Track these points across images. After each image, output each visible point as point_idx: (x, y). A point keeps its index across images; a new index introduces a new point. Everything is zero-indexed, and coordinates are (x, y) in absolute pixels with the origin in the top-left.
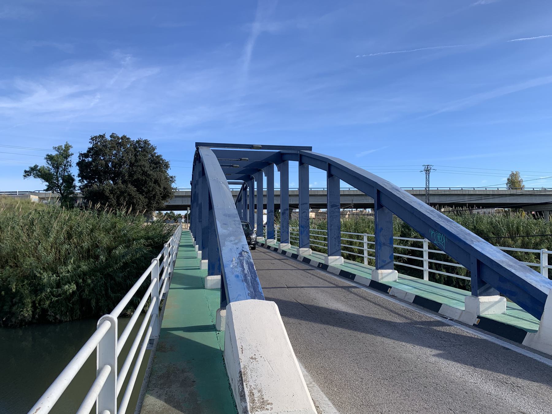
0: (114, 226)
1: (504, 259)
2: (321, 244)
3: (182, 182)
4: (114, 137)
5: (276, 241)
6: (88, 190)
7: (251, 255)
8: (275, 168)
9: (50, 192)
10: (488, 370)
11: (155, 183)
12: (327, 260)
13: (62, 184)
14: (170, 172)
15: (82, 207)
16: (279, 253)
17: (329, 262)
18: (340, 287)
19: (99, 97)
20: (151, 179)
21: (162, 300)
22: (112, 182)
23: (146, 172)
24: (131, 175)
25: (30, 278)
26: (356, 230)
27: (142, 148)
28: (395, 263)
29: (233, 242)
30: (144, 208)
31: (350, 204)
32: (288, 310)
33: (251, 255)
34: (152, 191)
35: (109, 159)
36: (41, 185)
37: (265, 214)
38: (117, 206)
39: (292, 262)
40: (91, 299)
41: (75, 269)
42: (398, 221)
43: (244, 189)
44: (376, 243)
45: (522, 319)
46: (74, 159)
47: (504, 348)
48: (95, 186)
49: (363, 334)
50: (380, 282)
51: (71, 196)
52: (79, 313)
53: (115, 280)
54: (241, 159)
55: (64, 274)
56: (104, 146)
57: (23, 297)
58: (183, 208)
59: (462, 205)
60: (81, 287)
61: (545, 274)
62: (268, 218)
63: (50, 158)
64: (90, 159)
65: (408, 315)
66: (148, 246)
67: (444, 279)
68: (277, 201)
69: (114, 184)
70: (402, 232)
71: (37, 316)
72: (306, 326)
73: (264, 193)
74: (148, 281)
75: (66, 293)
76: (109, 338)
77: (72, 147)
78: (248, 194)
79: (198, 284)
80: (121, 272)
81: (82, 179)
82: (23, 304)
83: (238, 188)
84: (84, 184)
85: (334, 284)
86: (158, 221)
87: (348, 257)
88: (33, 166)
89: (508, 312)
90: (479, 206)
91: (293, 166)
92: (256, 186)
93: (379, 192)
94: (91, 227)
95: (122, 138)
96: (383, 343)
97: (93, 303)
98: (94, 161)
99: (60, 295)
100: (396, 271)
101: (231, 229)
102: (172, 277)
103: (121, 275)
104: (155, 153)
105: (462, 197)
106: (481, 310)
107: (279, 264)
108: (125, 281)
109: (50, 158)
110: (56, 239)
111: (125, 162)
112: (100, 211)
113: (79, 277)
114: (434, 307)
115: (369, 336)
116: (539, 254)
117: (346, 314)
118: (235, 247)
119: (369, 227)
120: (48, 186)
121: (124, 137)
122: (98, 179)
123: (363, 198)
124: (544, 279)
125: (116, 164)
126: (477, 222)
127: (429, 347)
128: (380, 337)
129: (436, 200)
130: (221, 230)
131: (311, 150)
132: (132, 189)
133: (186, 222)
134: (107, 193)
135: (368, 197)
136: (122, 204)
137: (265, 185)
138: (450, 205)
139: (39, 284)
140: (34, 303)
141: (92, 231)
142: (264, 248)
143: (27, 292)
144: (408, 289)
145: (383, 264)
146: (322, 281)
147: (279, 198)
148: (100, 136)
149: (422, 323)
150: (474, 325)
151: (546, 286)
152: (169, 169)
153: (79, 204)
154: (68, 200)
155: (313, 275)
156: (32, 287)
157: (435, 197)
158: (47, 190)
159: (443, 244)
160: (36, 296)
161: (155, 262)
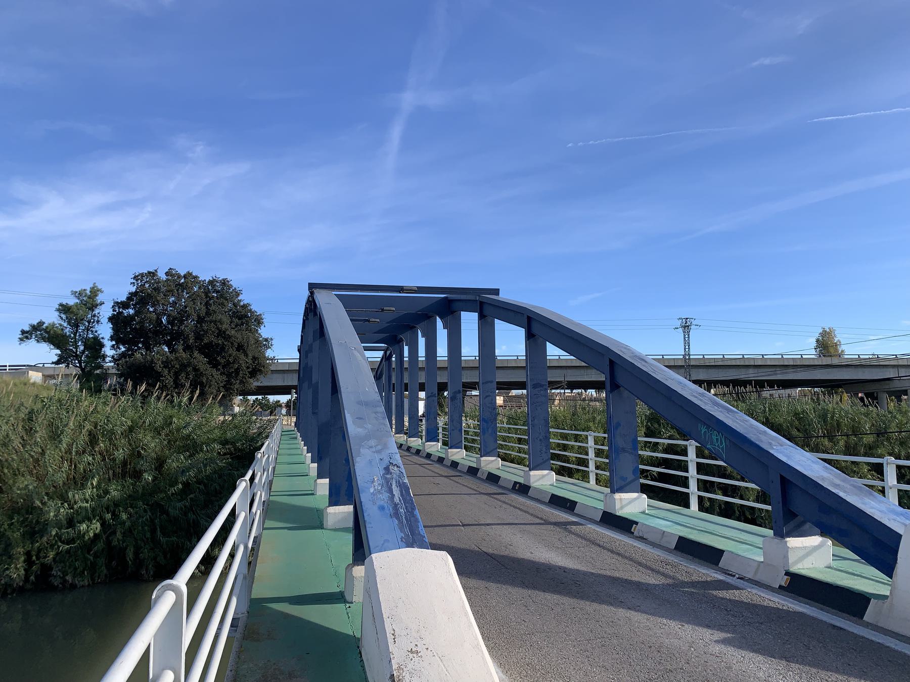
0: (168, 422)
1: (825, 474)
2: (513, 449)
3: (283, 346)
4: (172, 275)
5: (440, 444)
6: (126, 362)
7: (404, 471)
8: (439, 323)
9: (63, 366)
10: (809, 665)
11: (238, 349)
12: (528, 477)
13: (83, 352)
14: (264, 332)
15: (115, 390)
16: (447, 466)
17: (532, 481)
18: (551, 523)
19: (150, 209)
20: (232, 344)
21: (253, 549)
22: (166, 349)
23: (224, 332)
24: (198, 337)
25: (23, 511)
26: (574, 427)
27: (218, 292)
28: (642, 481)
29: (374, 449)
30: (219, 391)
32: (475, 566)
33: (404, 471)
34: (234, 362)
35: (161, 312)
36: (47, 354)
37: (422, 400)
38: (175, 388)
39: (469, 480)
40: (127, 546)
41: (99, 496)
42: (642, 409)
43: (387, 358)
44: (610, 448)
45: (861, 577)
46: (105, 312)
47: (834, 626)
48: (138, 355)
49: (595, 606)
50: (618, 514)
51: (98, 372)
52: (105, 571)
53: (168, 514)
54: (383, 310)
55: (80, 504)
56: (155, 289)
57: (11, 544)
58: (285, 390)
59: (744, 383)
60: (109, 525)
61: (893, 497)
62: (427, 406)
63: (64, 309)
64: (131, 311)
65: (669, 571)
66: (225, 454)
67: (720, 506)
68: (442, 378)
69: (171, 352)
70: (648, 428)
71: (32, 578)
72: (504, 595)
74: (233, 515)
75: (84, 537)
76: (173, 622)
77: (102, 292)
78: (394, 366)
79: (312, 520)
80: (180, 501)
81: (117, 343)
82: (10, 557)
83: (377, 356)
84: (119, 352)
85: (541, 519)
86: (242, 414)
87: (560, 471)
88: (35, 323)
89: (835, 564)
90: (772, 384)
91: (469, 321)
92: (406, 353)
93: (612, 363)
94: (129, 423)
95: (185, 277)
96: (630, 619)
97: (130, 554)
98: (137, 313)
99: (72, 541)
100: (645, 496)
101: (370, 426)
102: (270, 509)
103: (179, 505)
104: (240, 301)
105: (743, 370)
107: (446, 485)
108: (185, 514)
109: (64, 309)
110: (70, 446)
111: (188, 316)
112: (145, 398)
113: (104, 509)
114: (711, 556)
115: (605, 609)
117: (565, 570)
118: (377, 457)
120: (59, 356)
121: (188, 275)
122: (143, 343)
123: (582, 371)
124: (892, 507)
125: (175, 319)
126: (770, 410)
127: (708, 627)
128: (624, 611)
129: (702, 375)
130: (353, 428)
131: (498, 294)
132: (200, 360)
133: (288, 414)
134: (158, 367)
135: (589, 371)
136: (183, 386)
137: (422, 352)
138: (725, 383)
139: (38, 522)
140: (28, 554)
141: (131, 429)
142: (421, 457)
143: (17, 535)
144: (666, 527)
146: (519, 512)
147: (446, 373)
148: (149, 273)
149: (693, 584)
150: (781, 587)
151: (898, 519)
152: (262, 327)
153: (110, 385)
154: (91, 379)
155: (504, 502)
156: (26, 526)
157: (701, 370)
158: (57, 363)
159: (722, 449)
160: (32, 543)
161: (242, 485)
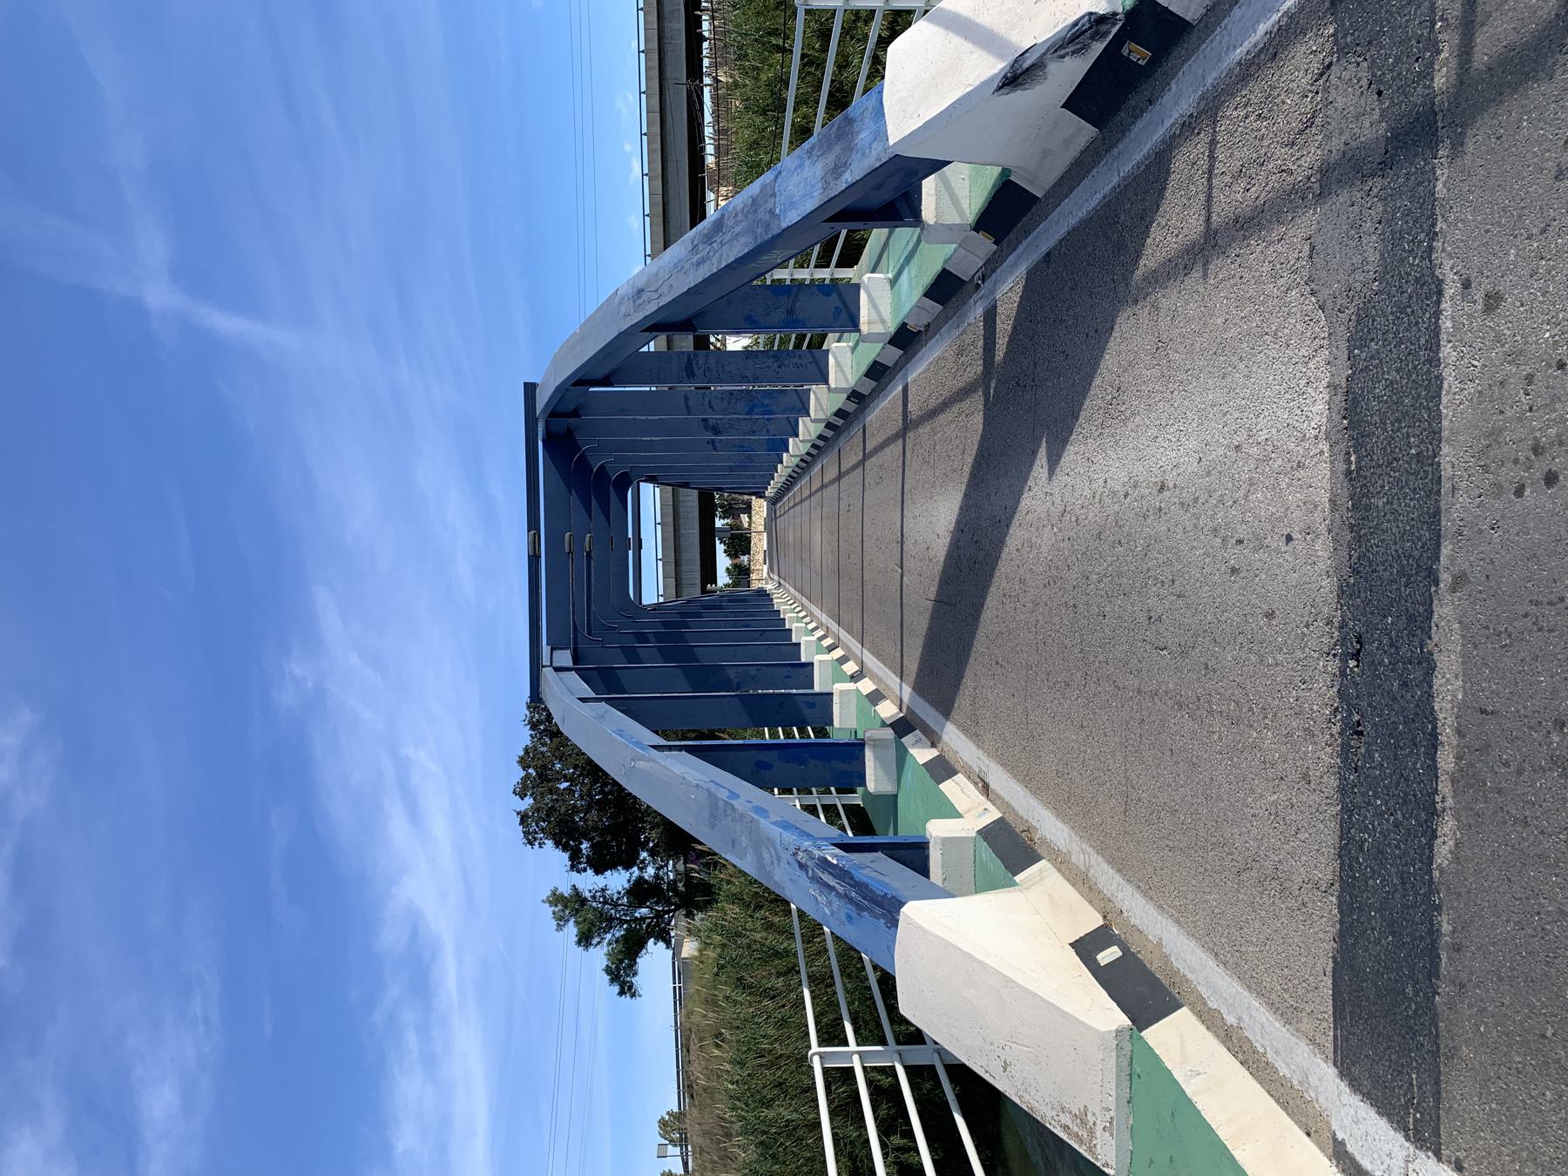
17: (845, 385)
31: (689, 92)
36: (655, 962)
46: (588, 882)
56: (548, 815)
62: (737, 331)
63: (585, 939)
64: (585, 846)
73: (663, 347)
106: (958, 221)
109: (585, 939)
116: (808, 12)
119: (701, 1040)
121: (523, 762)
145: (844, 315)
